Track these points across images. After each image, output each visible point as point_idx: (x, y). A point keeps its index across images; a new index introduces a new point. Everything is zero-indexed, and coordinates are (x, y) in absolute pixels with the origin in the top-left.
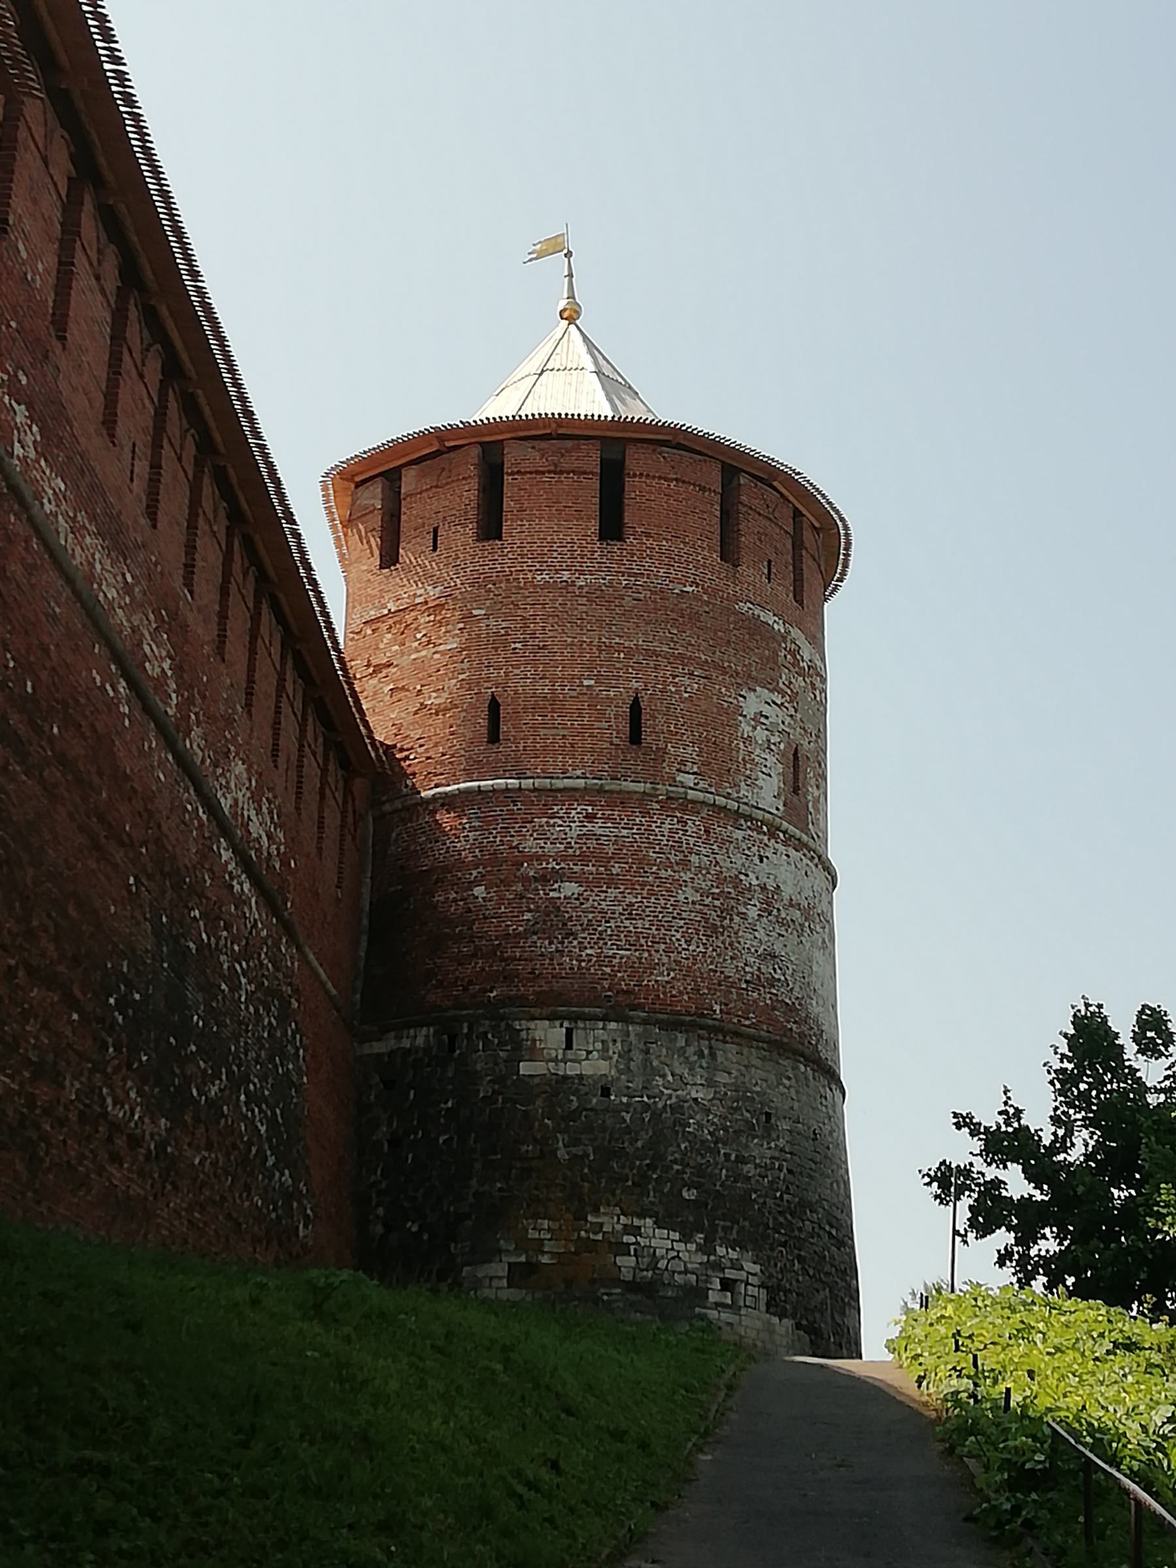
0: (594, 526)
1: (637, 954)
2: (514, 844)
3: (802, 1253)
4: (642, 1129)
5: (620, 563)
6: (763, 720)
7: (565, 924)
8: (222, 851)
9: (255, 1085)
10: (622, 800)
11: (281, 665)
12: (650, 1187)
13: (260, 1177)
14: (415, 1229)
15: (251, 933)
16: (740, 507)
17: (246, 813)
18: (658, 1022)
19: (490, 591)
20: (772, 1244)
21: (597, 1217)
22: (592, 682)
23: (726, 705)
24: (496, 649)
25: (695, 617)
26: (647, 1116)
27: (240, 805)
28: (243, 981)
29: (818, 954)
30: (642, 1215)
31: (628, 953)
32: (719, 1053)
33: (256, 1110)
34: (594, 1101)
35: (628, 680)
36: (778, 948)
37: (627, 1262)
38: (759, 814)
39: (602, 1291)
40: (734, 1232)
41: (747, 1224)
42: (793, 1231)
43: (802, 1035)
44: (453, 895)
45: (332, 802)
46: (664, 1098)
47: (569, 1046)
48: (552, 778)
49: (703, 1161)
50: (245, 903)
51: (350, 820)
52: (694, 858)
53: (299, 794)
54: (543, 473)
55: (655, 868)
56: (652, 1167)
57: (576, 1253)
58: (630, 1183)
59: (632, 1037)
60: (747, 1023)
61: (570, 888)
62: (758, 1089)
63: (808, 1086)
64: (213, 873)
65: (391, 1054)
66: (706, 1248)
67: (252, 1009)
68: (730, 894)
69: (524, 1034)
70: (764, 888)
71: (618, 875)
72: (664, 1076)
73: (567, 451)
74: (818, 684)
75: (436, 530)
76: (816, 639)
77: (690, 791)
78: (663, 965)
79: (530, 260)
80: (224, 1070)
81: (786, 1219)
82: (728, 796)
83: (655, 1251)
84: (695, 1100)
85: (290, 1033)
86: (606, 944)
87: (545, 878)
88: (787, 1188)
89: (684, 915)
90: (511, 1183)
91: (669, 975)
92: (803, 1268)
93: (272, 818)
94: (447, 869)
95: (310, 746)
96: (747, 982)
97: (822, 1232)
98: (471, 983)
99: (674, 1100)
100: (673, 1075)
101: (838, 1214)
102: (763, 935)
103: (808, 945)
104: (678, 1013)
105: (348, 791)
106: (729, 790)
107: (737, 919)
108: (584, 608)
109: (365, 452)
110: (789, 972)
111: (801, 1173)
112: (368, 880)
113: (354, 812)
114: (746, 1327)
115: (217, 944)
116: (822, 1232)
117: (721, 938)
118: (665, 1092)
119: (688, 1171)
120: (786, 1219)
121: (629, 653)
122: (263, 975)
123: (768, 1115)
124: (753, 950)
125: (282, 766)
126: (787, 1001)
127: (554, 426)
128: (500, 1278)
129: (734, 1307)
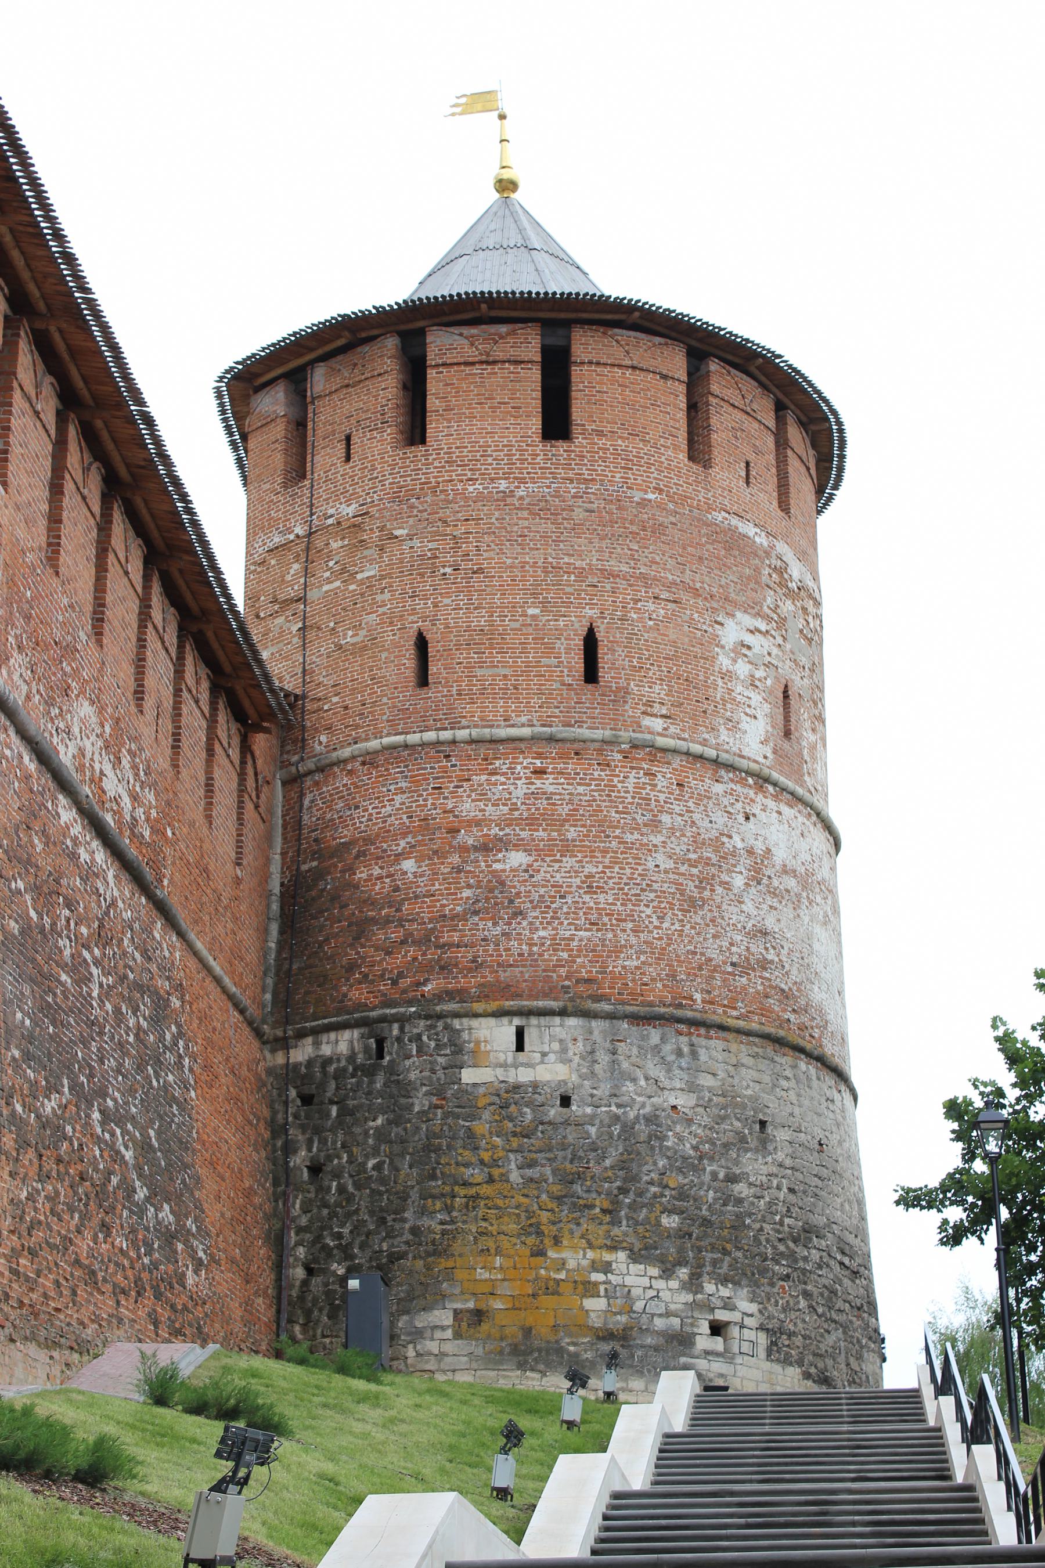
0: (536, 424)
1: (599, 934)
2: (450, 806)
3: (809, 1288)
4: (610, 1146)
5: (568, 467)
6: (744, 651)
7: (511, 902)
8: (60, 810)
9: (115, 1100)
10: (577, 749)
11: (144, 587)
12: (623, 1213)
13: (125, 1213)
14: (341, 1271)
15: (107, 913)
16: (711, 399)
17: (97, 766)
18: (626, 1016)
19: (412, 507)
20: (771, 1279)
21: (558, 1252)
22: (537, 611)
23: (699, 633)
24: (422, 575)
25: (658, 530)
26: (616, 1130)
27: (88, 756)
28: (95, 971)
29: (818, 929)
30: (613, 1248)
31: (589, 933)
32: (702, 1052)
33: (118, 1131)
34: (552, 1112)
35: (580, 606)
36: (770, 923)
37: (596, 1305)
38: (744, 764)
39: (567, 1340)
40: (725, 1265)
41: (739, 1254)
42: (796, 1261)
43: (802, 1028)
44: (377, 871)
45: (225, 761)
46: (637, 1107)
47: (520, 1047)
48: (492, 726)
49: (686, 1181)
50: (97, 875)
51: (250, 783)
52: (665, 818)
53: (176, 747)
54: (473, 364)
55: (618, 832)
56: (623, 1191)
57: (534, 1295)
58: (598, 1210)
59: (596, 1033)
60: (735, 1013)
61: (517, 859)
62: (749, 1092)
63: (810, 1087)
64: (48, 837)
65: (310, 1063)
66: (693, 1284)
67: (109, 1007)
68: (710, 861)
69: (465, 1036)
70: (750, 852)
71: (574, 840)
72: (634, 1080)
73: (502, 337)
74: (811, 609)
75: (348, 438)
76: (808, 554)
77: (658, 738)
78: (631, 947)
79: (453, 114)
80: (65, 1082)
81: (787, 1247)
82: (704, 743)
83: (629, 1291)
84: (674, 1107)
85: (168, 1036)
86: (562, 923)
87: (485, 848)
88: (789, 1210)
89: (655, 886)
90: (455, 1214)
91: (638, 958)
92: (810, 1306)
93: (137, 775)
94: (369, 841)
95: (190, 691)
96: (733, 964)
97: (832, 1263)
98: (401, 975)
99: (648, 1109)
100: (647, 1079)
101: (850, 1238)
102: (753, 909)
103: (806, 919)
104: (651, 1004)
105: (246, 748)
106: (706, 736)
107: (719, 890)
108: (526, 523)
109: (264, 349)
110: (784, 952)
111: (804, 1192)
112: (278, 857)
113: (256, 774)
114: (742, 1378)
115: (54, 924)
116: (832, 1263)
117: (701, 913)
118: (638, 1098)
119: (667, 1192)
120: (787, 1247)
121: (581, 574)
122: (126, 966)
123: (763, 1124)
124: (739, 926)
125: (150, 713)
126: (783, 986)
127: (484, 306)
128: (443, 1328)
129: (727, 1356)
